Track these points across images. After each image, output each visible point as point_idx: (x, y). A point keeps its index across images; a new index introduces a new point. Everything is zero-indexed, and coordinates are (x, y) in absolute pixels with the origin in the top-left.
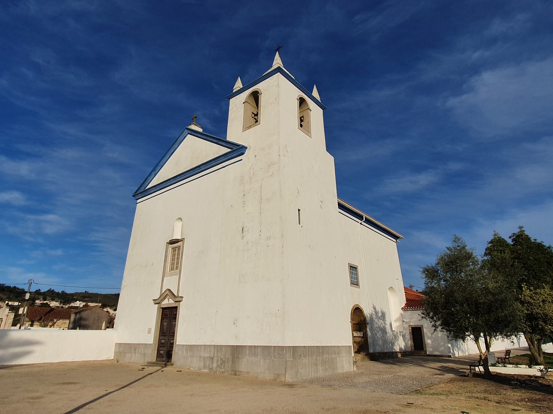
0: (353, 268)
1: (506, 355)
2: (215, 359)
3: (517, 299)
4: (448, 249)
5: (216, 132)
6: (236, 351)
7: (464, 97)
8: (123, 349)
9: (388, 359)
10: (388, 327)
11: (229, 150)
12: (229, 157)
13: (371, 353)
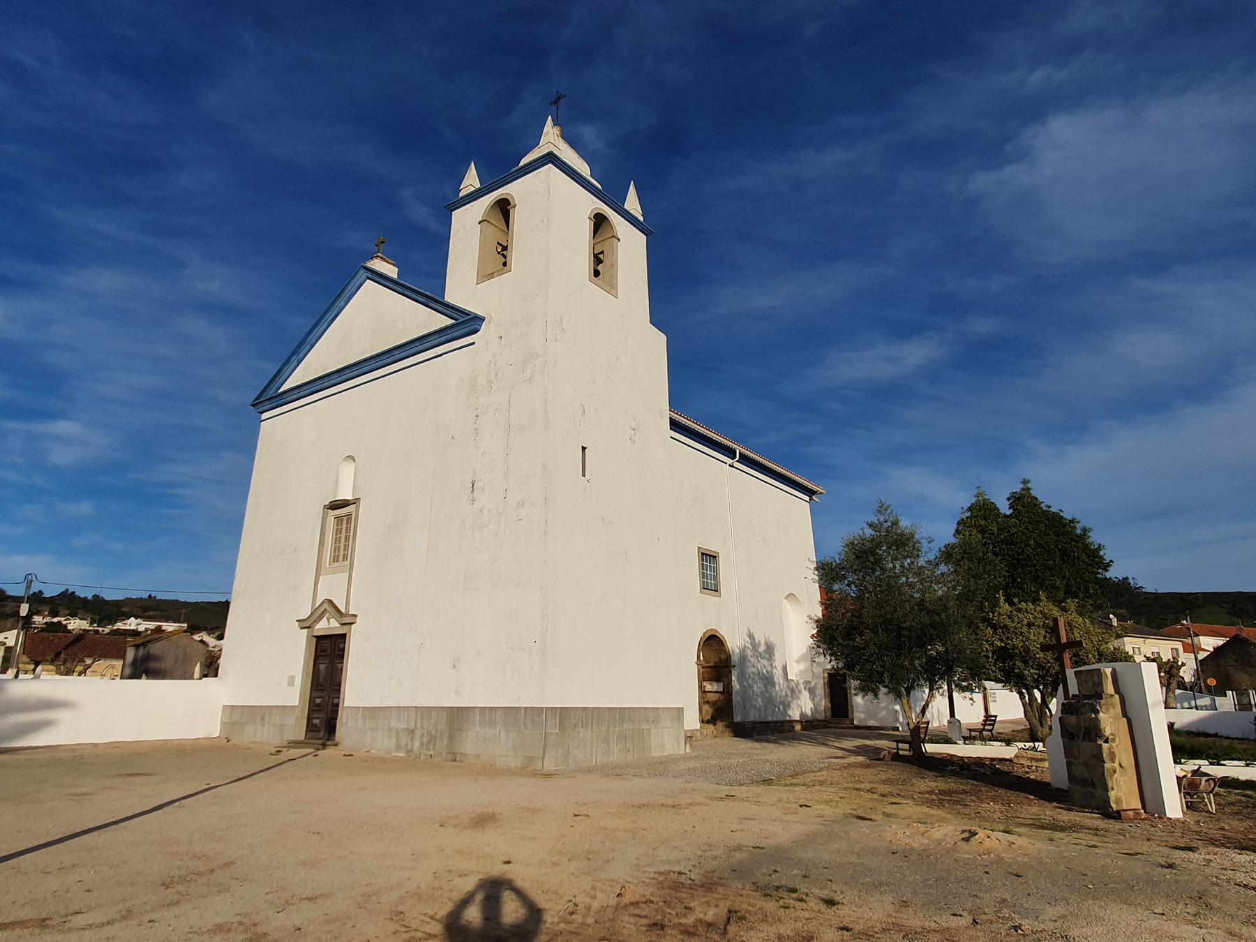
0: (708, 558)
1: (984, 725)
2: (417, 736)
3: (986, 620)
4: (871, 525)
5: (423, 283)
6: (457, 717)
7: (1008, 171)
8: (238, 716)
9: (772, 734)
10: (778, 673)
11: (451, 321)
12: (449, 337)
13: (738, 724)
